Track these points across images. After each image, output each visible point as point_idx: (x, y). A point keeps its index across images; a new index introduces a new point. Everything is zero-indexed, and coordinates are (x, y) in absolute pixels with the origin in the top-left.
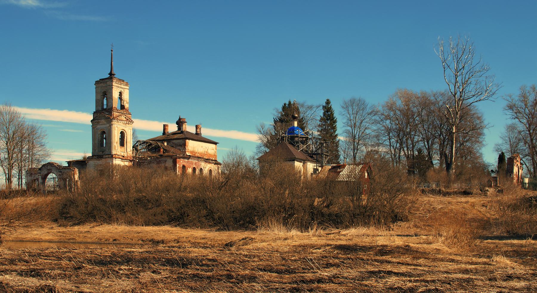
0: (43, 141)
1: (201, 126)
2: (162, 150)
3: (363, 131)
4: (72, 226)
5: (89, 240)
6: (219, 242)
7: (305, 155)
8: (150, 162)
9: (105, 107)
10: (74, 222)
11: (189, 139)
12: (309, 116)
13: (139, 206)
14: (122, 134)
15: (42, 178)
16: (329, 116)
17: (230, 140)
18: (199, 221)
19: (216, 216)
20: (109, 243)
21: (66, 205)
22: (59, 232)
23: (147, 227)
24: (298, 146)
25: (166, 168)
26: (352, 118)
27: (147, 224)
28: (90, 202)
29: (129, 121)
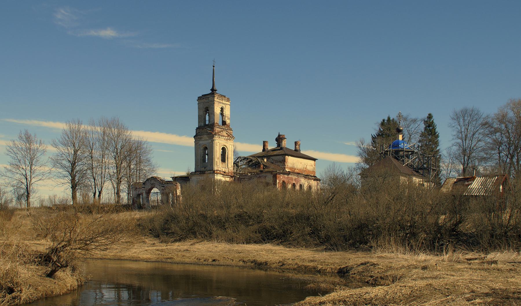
0: (149, 156)
1: (300, 142)
2: (262, 166)
3: (475, 143)
4: (173, 242)
5: (187, 260)
6: (332, 267)
7: (410, 169)
8: (250, 178)
9: (207, 123)
10: (175, 238)
11: (289, 155)
12: (413, 129)
13: (240, 222)
14: (224, 149)
15: (146, 193)
16: (430, 130)
17: (328, 156)
18: (304, 240)
19: (323, 234)
20: (207, 265)
21: (168, 220)
22: (158, 250)
23: (248, 246)
24: (403, 160)
25: (268, 184)
26: (463, 130)
27: (248, 242)
28: (191, 218)
29: (230, 137)
